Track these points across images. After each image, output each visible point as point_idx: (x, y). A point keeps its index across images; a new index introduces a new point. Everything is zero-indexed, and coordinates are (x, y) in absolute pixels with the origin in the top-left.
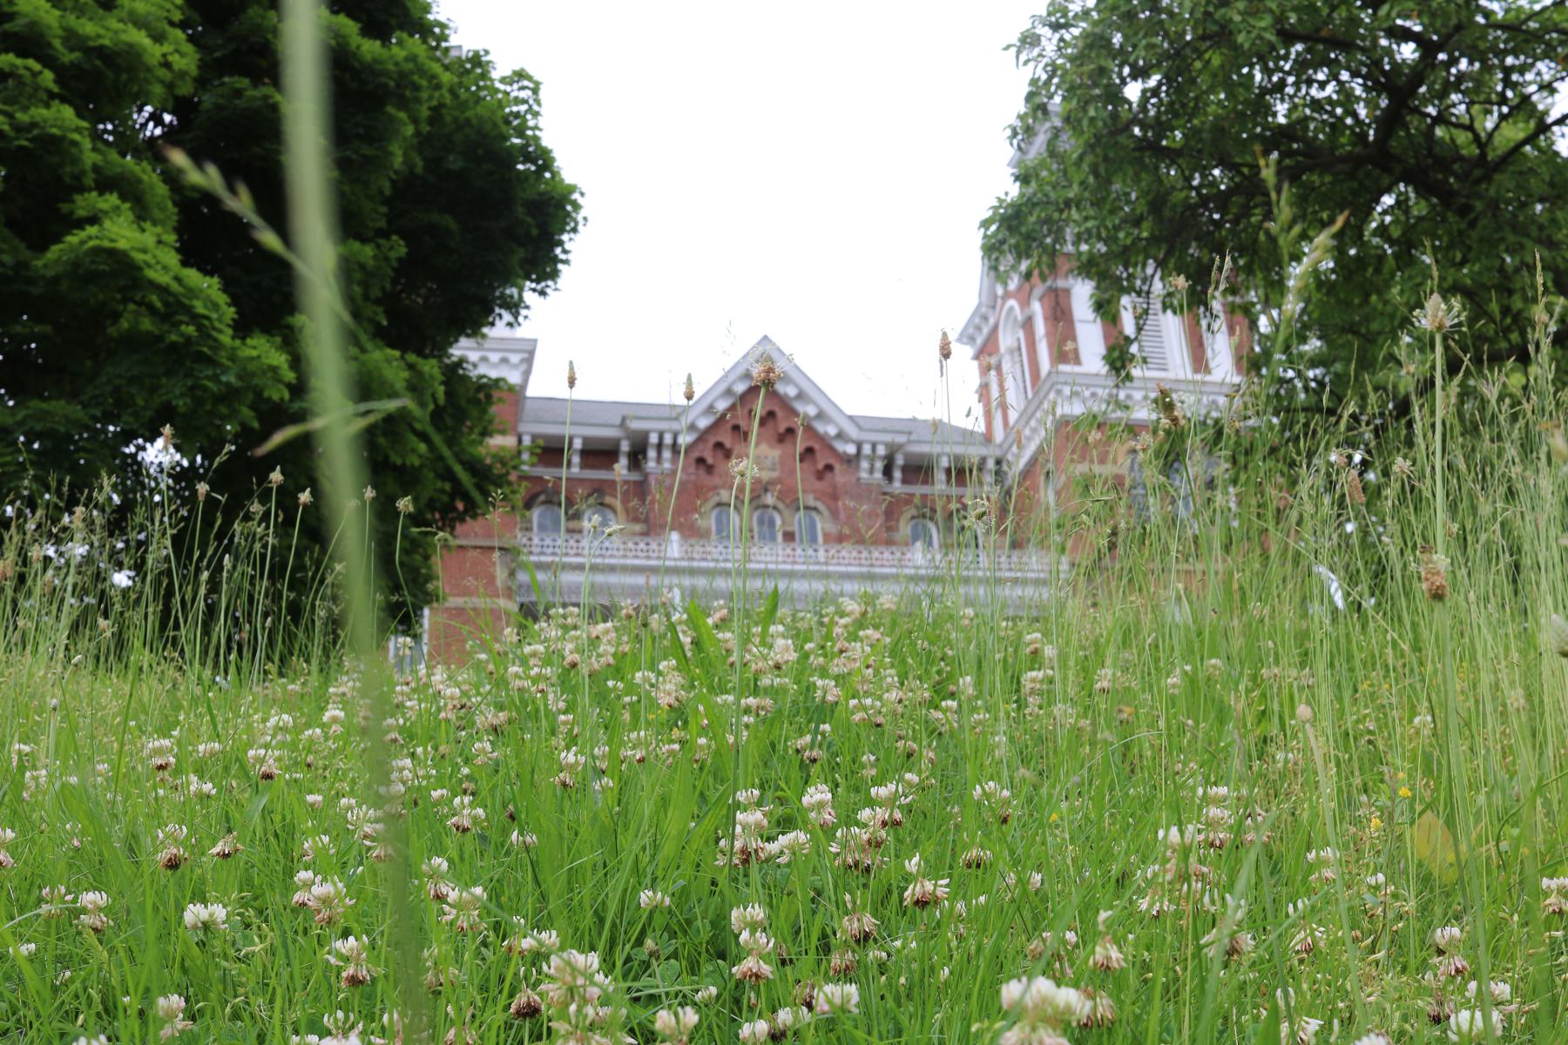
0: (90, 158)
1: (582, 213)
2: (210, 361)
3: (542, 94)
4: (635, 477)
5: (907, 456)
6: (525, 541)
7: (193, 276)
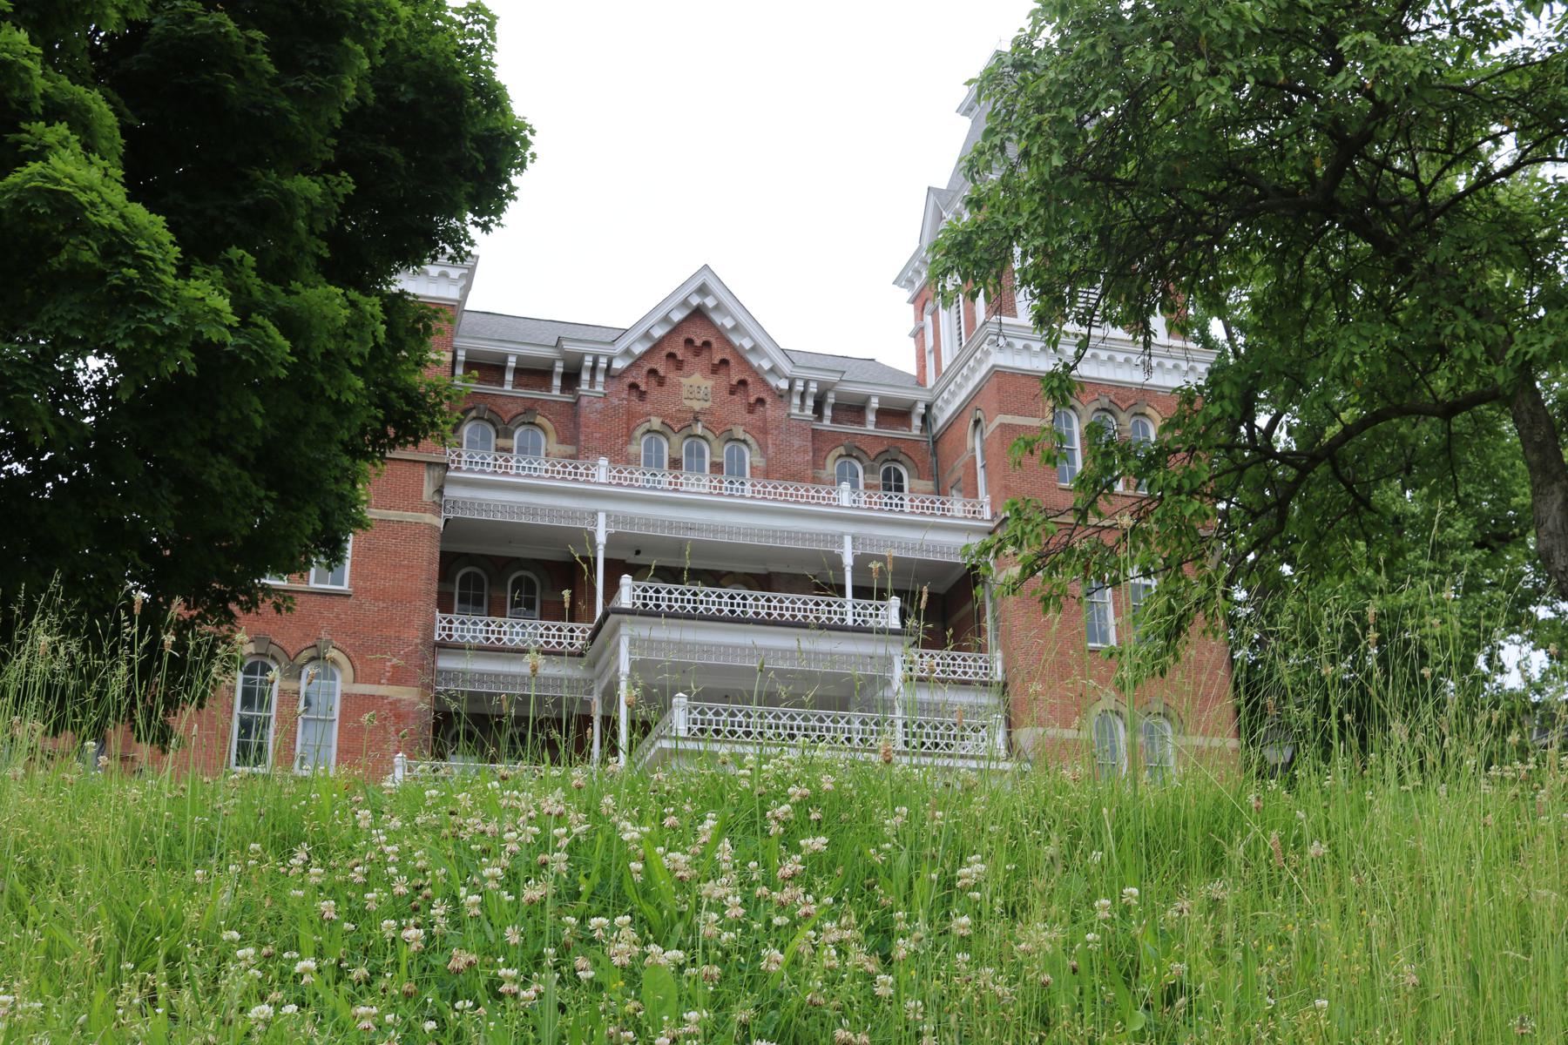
0: (40, 84)
1: (531, 149)
2: (153, 303)
3: (498, 29)
4: (568, 398)
5: (838, 395)
6: (454, 457)
7: (138, 212)
